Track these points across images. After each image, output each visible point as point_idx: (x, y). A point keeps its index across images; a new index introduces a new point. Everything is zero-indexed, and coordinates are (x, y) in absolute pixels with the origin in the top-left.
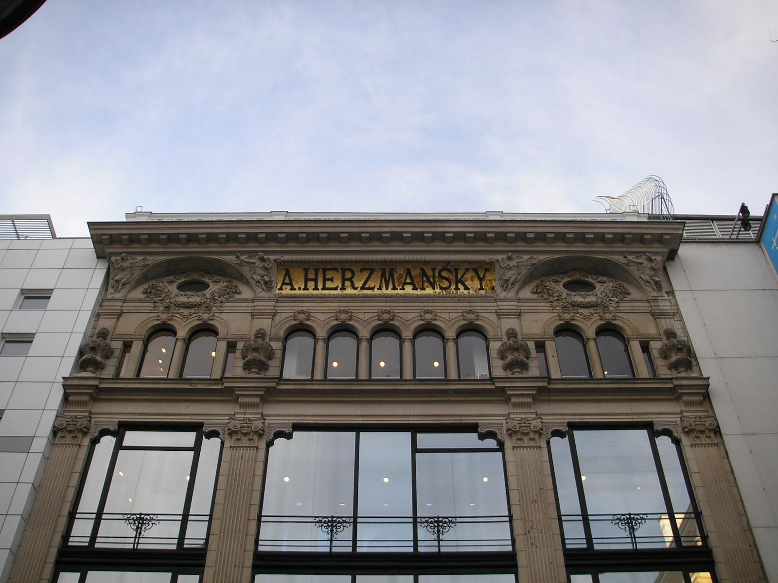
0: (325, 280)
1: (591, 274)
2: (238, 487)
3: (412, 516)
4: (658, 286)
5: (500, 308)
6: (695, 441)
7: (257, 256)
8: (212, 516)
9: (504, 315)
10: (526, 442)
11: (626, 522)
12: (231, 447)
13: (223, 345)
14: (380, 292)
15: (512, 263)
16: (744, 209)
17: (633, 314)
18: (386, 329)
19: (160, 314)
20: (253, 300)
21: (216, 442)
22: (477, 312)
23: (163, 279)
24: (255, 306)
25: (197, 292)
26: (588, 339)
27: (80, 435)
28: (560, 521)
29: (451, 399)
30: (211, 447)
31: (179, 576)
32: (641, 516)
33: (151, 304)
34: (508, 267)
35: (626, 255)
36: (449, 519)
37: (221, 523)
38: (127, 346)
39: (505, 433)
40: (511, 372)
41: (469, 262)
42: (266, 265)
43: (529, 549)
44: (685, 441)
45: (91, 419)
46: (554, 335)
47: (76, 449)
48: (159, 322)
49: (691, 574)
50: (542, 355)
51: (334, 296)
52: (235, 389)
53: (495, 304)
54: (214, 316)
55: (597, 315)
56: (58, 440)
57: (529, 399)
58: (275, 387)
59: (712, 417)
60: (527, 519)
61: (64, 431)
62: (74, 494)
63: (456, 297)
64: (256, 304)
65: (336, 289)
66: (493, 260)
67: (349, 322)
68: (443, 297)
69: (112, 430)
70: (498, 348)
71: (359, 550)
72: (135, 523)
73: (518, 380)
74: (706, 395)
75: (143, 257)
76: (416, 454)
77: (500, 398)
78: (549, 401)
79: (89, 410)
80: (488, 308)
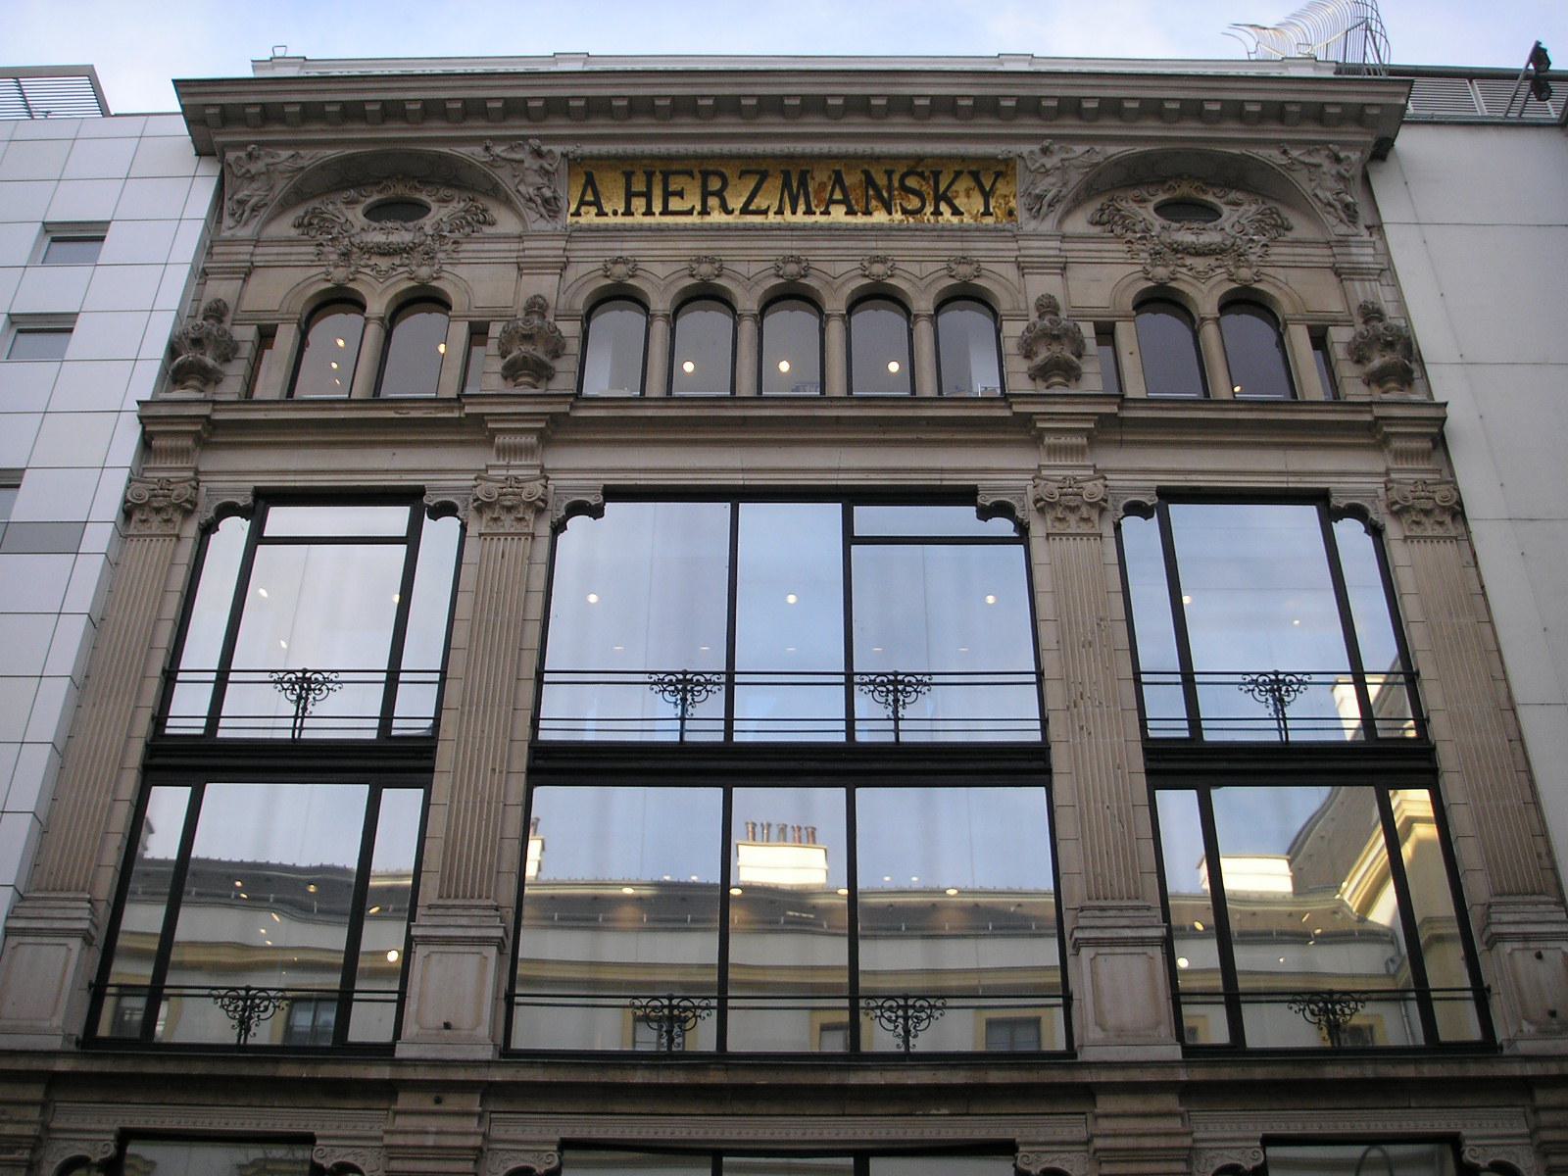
0: (667, 195)
1: (1213, 185)
2: (496, 614)
3: (843, 670)
4: (1351, 213)
5: (1023, 252)
7: (527, 147)
9: (1033, 268)
10: (1073, 525)
12: (481, 535)
13: (460, 331)
14: (779, 219)
15: (1050, 162)
16: (1539, 55)
17: (1298, 270)
18: (792, 294)
19: (331, 269)
20: (520, 238)
21: (450, 525)
22: (978, 261)
23: (333, 197)
24: (524, 250)
25: (405, 222)
26: (1203, 319)
27: (177, 517)
30: (440, 535)
32: (1299, 677)
33: (312, 249)
34: (1043, 170)
35: (1288, 148)
38: (266, 336)
39: (1032, 506)
40: (1045, 385)
41: (963, 158)
42: (547, 166)
44: (1393, 531)
46: (1134, 309)
48: (329, 285)
49: (1391, 792)
50: (1109, 349)
51: (685, 228)
53: (1013, 245)
54: (440, 270)
55: (1223, 270)
59: (1448, 482)
61: (147, 509)
62: (171, 636)
63: (935, 230)
64: (526, 244)
65: (690, 212)
66: (1011, 155)
67: (718, 281)
68: (908, 229)
70: (1020, 334)
71: (737, 738)
73: (1057, 400)
75: (292, 152)
76: (853, 547)
77: (1021, 437)
78: (1122, 443)
80: (1000, 253)
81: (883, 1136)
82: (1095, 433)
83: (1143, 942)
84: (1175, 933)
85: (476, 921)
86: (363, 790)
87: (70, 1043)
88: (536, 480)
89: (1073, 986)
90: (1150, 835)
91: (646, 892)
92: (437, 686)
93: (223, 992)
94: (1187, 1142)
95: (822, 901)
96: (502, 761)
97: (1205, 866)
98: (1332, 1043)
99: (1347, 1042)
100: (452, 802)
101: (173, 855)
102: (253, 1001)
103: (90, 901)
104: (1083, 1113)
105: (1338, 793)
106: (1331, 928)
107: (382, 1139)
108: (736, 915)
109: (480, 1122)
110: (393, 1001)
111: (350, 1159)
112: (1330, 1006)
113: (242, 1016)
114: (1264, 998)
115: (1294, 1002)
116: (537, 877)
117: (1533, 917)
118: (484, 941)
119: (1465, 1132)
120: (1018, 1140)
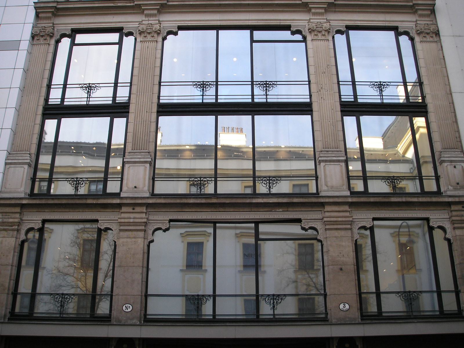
2: (146, 65)
6: (423, 39)
8: (132, 83)
10: (320, 36)
11: (378, 86)
12: (141, 41)
21: (131, 39)
27: (48, 38)
28: (339, 85)
29: (275, 9)
30: (129, 42)
31: (115, 119)
32: (387, 83)
36: (273, 82)
37: (137, 88)
43: (319, 100)
44: (417, 39)
45: (54, 28)
47: (47, 46)
52: (141, 5)
56: (36, 42)
57: (322, 10)
58: (166, 4)
59: (435, 24)
60: (319, 83)
61: (39, 36)
69: (68, 34)
71: (219, 101)
72: (86, 89)
74: (433, 10)
76: (253, 43)
77: (304, 10)
78: (335, 12)
79: (52, 22)
81: (263, 217)
82: (327, 8)
83: (339, 161)
84: (348, 160)
85: (143, 156)
86: (108, 119)
87: (26, 195)
88: (157, 24)
89: (318, 174)
90: (336, 73)
91: (193, 148)
92: (129, 87)
93: (70, 179)
94: (351, 219)
95: (244, 150)
96: (149, 109)
97: (358, 140)
98: (394, 191)
99: (398, 191)
100: (135, 121)
101: (53, 141)
102: (78, 182)
103: (29, 154)
104: (321, 211)
105: (398, 118)
106: (394, 159)
107: (118, 220)
108: (219, 154)
109: (146, 215)
110: (119, 180)
111: (108, 226)
112: (393, 181)
113: (76, 186)
114: (374, 178)
115: (383, 179)
116: (160, 144)
117: (454, 156)
118: (146, 162)
119: (431, 217)
120: (302, 218)
